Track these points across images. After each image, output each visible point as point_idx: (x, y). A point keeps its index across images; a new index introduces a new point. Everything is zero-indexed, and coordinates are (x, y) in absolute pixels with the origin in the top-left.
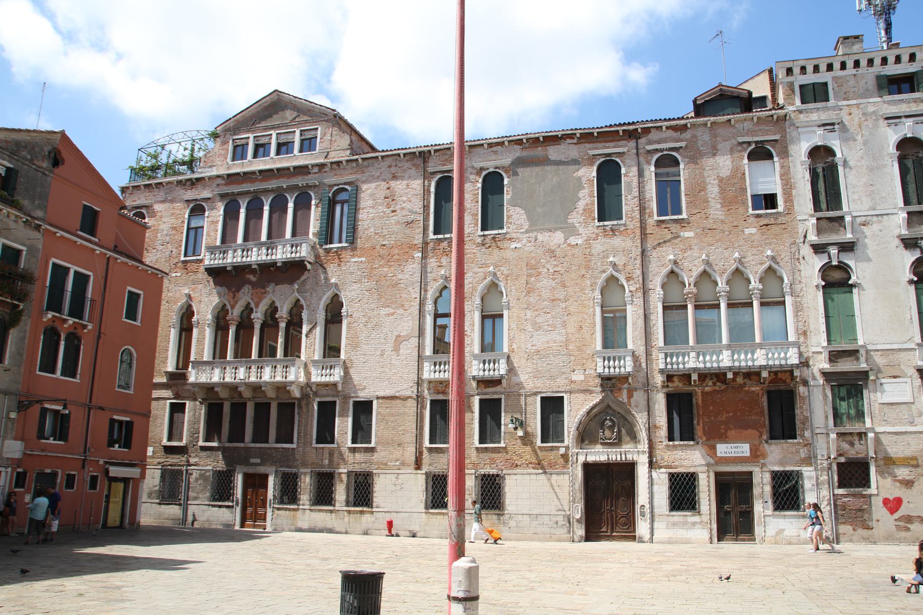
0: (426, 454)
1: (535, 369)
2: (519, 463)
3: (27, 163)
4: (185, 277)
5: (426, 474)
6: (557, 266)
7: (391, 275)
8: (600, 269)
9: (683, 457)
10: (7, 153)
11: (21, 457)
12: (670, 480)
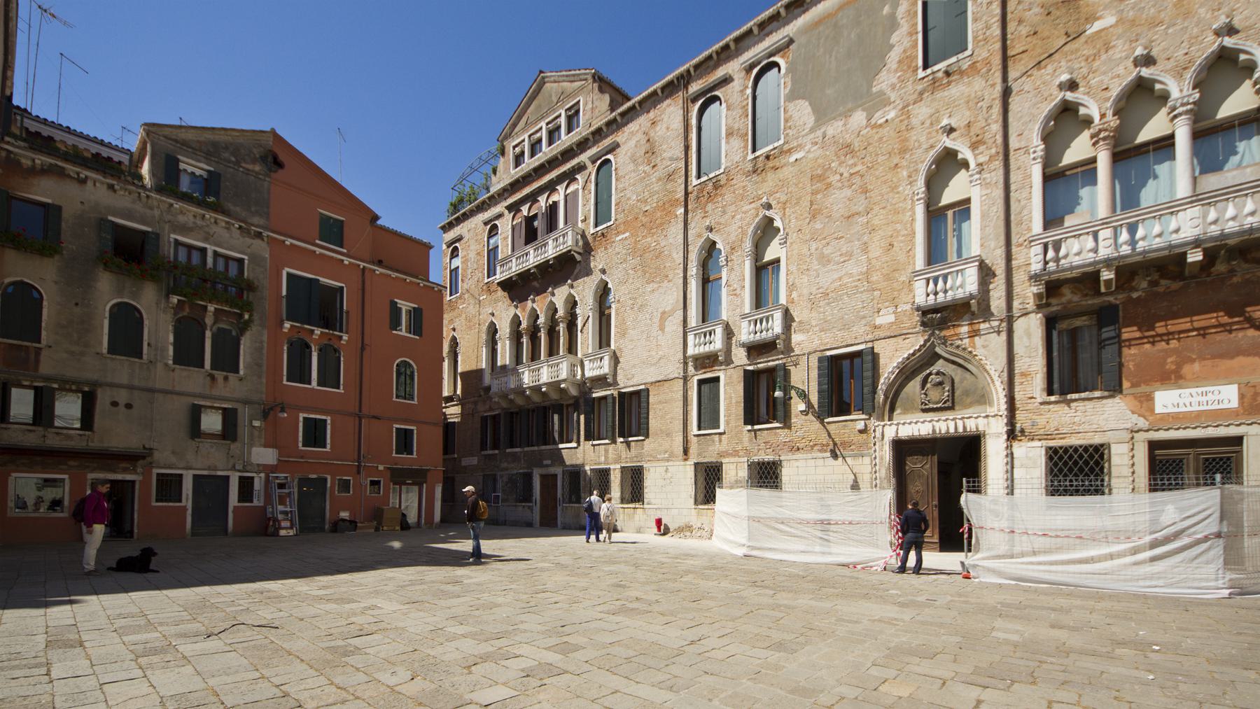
0: (693, 440)
1: (821, 319)
2: (801, 446)
3: (232, 165)
4: (489, 297)
5: (696, 465)
6: (855, 165)
7: (654, 244)
8: (925, 146)
9: (1076, 419)
10: (202, 154)
11: (275, 463)
12: (1050, 458)
